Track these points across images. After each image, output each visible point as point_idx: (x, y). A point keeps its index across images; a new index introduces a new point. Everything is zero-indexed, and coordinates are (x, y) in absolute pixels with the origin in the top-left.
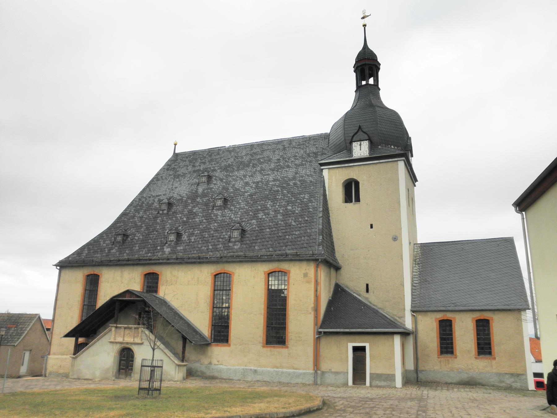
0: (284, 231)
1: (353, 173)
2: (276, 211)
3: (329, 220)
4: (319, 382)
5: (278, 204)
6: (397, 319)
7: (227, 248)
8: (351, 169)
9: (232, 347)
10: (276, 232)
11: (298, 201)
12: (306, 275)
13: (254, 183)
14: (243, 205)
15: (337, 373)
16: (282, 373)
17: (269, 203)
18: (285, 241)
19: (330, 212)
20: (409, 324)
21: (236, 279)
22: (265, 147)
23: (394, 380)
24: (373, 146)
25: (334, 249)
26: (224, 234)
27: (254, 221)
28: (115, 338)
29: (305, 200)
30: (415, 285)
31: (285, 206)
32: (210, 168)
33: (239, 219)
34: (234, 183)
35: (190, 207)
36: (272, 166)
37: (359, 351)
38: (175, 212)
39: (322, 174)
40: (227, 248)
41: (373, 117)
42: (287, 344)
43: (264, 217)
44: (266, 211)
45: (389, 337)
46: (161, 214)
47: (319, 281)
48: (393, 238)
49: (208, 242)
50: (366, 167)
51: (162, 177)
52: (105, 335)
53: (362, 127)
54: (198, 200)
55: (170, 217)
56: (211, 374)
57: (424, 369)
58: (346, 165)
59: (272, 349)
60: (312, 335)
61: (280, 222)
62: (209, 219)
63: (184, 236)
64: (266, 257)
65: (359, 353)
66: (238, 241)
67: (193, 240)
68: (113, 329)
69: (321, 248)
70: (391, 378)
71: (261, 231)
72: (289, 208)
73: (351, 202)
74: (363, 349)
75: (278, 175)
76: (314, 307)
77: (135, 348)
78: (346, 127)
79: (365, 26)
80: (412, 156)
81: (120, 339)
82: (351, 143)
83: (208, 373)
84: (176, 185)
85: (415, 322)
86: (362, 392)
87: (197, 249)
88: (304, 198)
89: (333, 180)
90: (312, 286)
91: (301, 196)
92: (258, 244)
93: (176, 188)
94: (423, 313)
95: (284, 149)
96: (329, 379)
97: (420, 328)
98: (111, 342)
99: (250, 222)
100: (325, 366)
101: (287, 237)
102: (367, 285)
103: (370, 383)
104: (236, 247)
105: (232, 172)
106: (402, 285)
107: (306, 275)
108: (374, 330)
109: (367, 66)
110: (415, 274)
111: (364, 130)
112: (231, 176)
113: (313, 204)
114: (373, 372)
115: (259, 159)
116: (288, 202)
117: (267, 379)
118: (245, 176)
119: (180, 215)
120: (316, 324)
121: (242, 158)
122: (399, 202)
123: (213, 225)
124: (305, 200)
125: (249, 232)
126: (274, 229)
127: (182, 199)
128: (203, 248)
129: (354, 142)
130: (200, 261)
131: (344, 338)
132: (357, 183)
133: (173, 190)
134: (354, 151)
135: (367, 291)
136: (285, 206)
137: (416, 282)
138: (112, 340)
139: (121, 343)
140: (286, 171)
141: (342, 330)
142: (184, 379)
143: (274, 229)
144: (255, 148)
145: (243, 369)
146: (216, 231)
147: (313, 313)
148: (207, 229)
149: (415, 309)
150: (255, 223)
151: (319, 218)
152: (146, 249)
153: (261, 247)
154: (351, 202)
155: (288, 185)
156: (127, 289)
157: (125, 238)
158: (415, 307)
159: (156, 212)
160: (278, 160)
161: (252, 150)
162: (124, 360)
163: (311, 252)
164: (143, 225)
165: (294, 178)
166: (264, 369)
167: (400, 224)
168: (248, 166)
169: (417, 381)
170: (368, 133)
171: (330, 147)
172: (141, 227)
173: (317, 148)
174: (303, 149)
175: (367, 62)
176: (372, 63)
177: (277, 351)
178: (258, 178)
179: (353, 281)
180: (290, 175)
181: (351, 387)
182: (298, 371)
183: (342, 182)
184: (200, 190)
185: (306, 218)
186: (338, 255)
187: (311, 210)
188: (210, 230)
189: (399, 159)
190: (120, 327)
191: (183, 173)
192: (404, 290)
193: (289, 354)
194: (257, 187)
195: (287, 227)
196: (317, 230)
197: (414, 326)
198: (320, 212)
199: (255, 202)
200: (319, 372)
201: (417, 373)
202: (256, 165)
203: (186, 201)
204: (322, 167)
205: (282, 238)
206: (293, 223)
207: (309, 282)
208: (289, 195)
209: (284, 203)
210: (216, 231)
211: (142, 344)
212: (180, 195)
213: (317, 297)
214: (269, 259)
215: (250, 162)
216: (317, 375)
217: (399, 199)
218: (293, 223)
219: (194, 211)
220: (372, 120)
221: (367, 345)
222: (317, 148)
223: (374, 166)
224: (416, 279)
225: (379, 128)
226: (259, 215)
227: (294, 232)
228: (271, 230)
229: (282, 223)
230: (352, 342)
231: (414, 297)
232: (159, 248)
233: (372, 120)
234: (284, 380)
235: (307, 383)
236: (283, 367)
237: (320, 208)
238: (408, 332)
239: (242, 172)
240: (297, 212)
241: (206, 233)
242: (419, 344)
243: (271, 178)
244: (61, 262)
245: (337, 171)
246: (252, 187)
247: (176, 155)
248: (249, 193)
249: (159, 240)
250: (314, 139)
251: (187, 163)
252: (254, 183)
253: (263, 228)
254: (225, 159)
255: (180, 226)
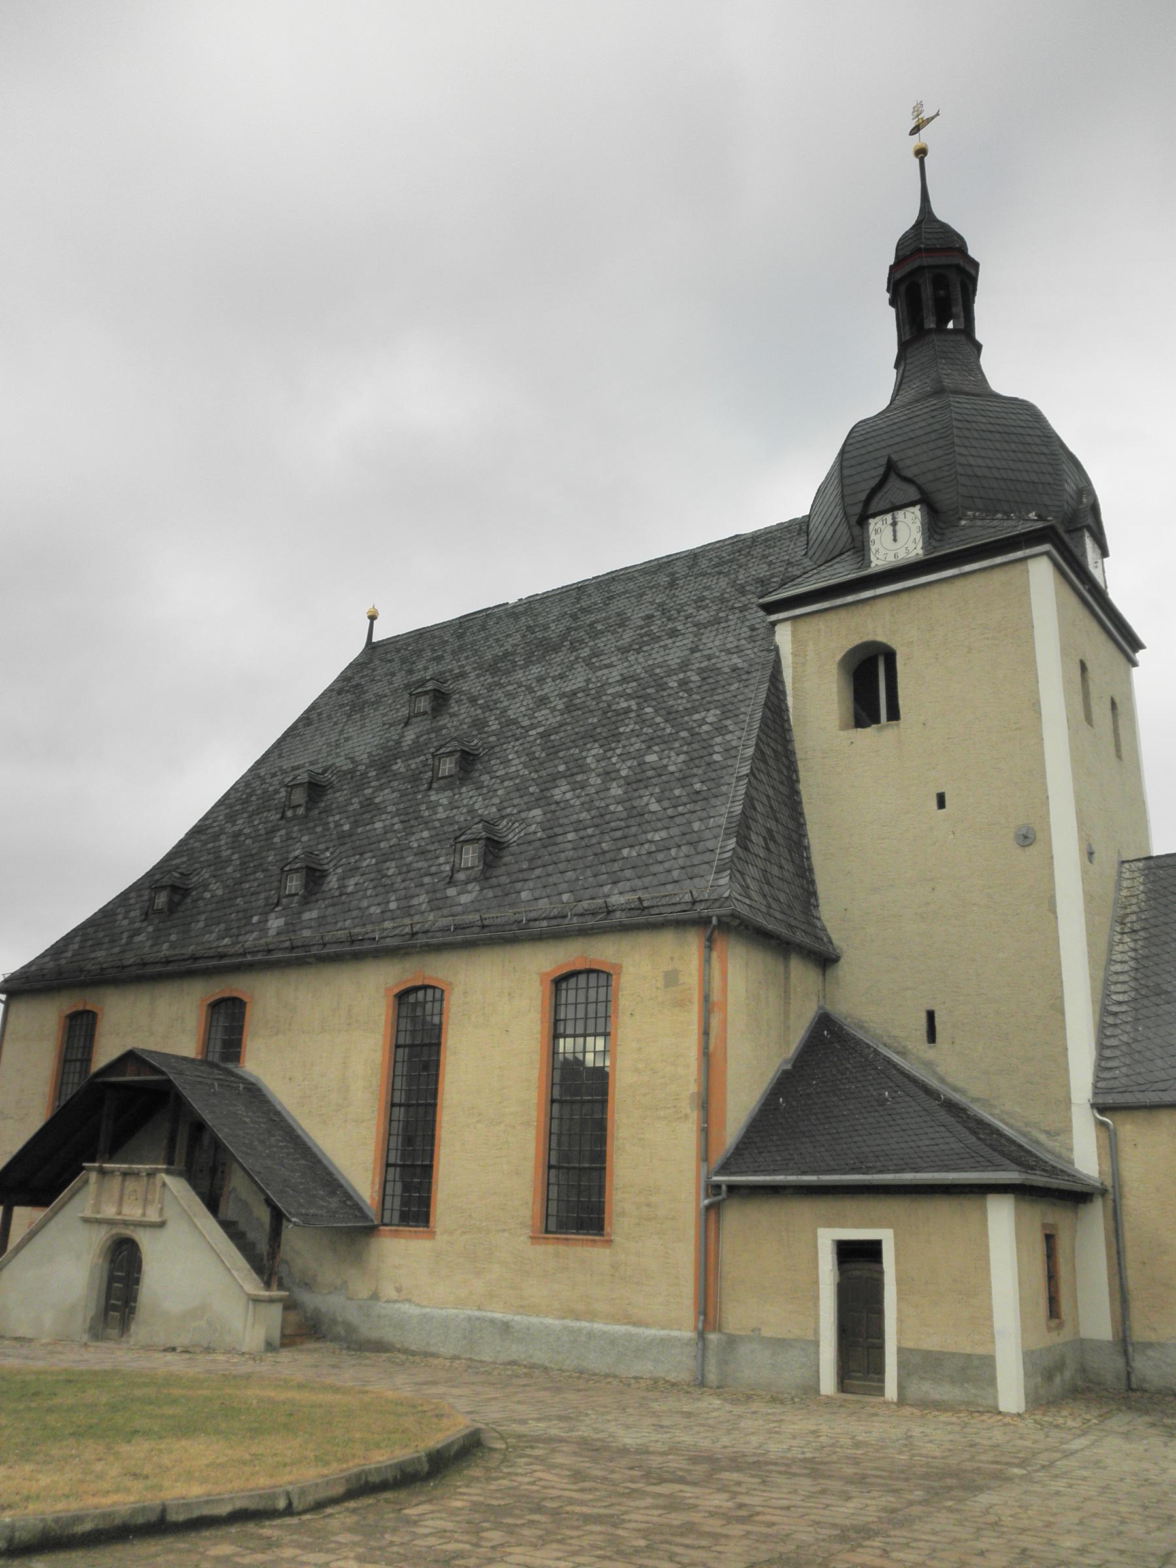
0: (619, 834)
1: (874, 622)
2: (609, 775)
3: (797, 793)
4: (712, 1377)
5: (618, 751)
6: (1043, 1138)
7: (438, 903)
8: (867, 609)
9: (441, 1239)
10: (594, 840)
11: (683, 734)
12: (671, 979)
13: (562, 695)
14: (516, 764)
15: (780, 1344)
16: (591, 1335)
17: (593, 752)
18: (616, 866)
19: (800, 765)
20: (1085, 1158)
21: (455, 1005)
22: (618, 588)
23: (992, 1381)
24: (937, 521)
25: (814, 894)
26: (442, 860)
27: (537, 812)
28: (97, 1207)
29: (705, 728)
30: (1115, 1009)
31: (640, 754)
32: (451, 671)
33: (494, 809)
34: (506, 703)
35: (368, 791)
36: (628, 637)
37: (858, 1257)
38: (327, 811)
39: (772, 642)
40: (438, 903)
41: (937, 426)
42: (607, 1229)
43: (569, 796)
44: (579, 778)
45: (968, 1204)
46: (289, 820)
47: (715, 997)
48: (1017, 835)
49: (390, 889)
50: (918, 596)
51: (320, 714)
52: (70, 1198)
53: (901, 464)
54: (395, 767)
55: (311, 825)
56: (374, 1335)
57: (1153, 1337)
58: (850, 599)
59: (562, 1248)
60: (692, 1198)
61: (612, 808)
62: (410, 818)
63: (329, 879)
64: (545, 923)
65: (860, 1269)
66: (475, 880)
67: (350, 889)
68: (93, 1176)
69: (724, 881)
70: (978, 1370)
71: (551, 839)
72: (651, 758)
73: (877, 720)
74: (870, 1252)
75: (637, 664)
76: (699, 1093)
77: (147, 1242)
78: (846, 472)
79: (921, 153)
80: (1104, 553)
81: (109, 1211)
82: (863, 520)
83: (367, 1331)
84: (351, 730)
85: (1111, 1148)
86: (878, 1428)
87: (355, 913)
88: (703, 722)
89: (810, 658)
90: (693, 1016)
91: (696, 717)
92: (531, 884)
93: (347, 739)
94: (1140, 1115)
95: (672, 584)
96: (753, 1365)
97: (1133, 1171)
98: (86, 1220)
99: (523, 815)
100: (738, 1315)
101: (625, 852)
102: (931, 1015)
103: (901, 1387)
104: (464, 899)
105: (508, 673)
106: (1058, 1008)
107: (671, 979)
108: (908, 1177)
109: (933, 283)
110: (1118, 967)
111: (907, 473)
112: (502, 686)
113: (728, 737)
114: (910, 1344)
115: (591, 625)
116: (650, 742)
117: (540, 1356)
118: (541, 680)
119: (337, 817)
120: (705, 1155)
121: (546, 627)
122: (1035, 706)
123: (417, 836)
124: (705, 728)
125: (514, 849)
126: (590, 831)
127: (352, 772)
128: (372, 910)
129: (874, 516)
130: (355, 952)
131: (802, 1211)
132: (890, 656)
133: (338, 746)
134: (873, 548)
135: (932, 1036)
136: (640, 754)
137: (1120, 998)
138: (88, 1213)
139: (110, 1222)
140: (665, 647)
141: (792, 1178)
142: (270, 1347)
143: (590, 831)
144: (590, 595)
145: (470, 1319)
146: (422, 853)
147: (694, 1115)
148: (401, 849)
149: (1109, 1100)
150: (539, 819)
151: (739, 779)
152: (222, 926)
153: (537, 894)
154: (877, 720)
155: (662, 687)
156: (129, 1048)
157: (177, 898)
158: (1109, 1091)
159: (279, 816)
160: (650, 617)
161: (578, 600)
162: (119, 1280)
163: (688, 898)
164: (236, 856)
165: (684, 666)
166: (534, 1320)
167: (1044, 784)
168: (556, 649)
169: (1130, 1388)
170: (920, 480)
171: (810, 553)
172: (229, 860)
173: (770, 564)
174: (727, 575)
175: (927, 261)
176: (943, 260)
177: (581, 1252)
178: (578, 679)
179: (877, 1000)
180: (674, 657)
181: (828, 1401)
182: (641, 1330)
183: (839, 657)
184: (410, 736)
185: (697, 786)
186: (829, 912)
187: (717, 757)
188: (405, 854)
189: (1028, 552)
190: (112, 1172)
191: (376, 695)
192: (1064, 1028)
193: (615, 1267)
194: (569, 708)
195: (632, 821)
196: (723, 821)
197: (1107, 1168)
198: (743, 760)
199: (553, 752)
200: (713, 1337)
201: (1125, 1353)
202: (582, 641)
203: (364, 774)
204: (774, 618)
205: (608, 856)
206: (654, 807)
207: (681, 1004)
208: (658, 720)
209: (637, 746)
210: (422, 853)
211: (162, 1225)
212: (353, 760)
213: (710, 1061)
214: (554, 932)
215: (563, 638)
216: (704, 1349)
217: (1037, 692)
218: (654, 807)
219: (377, 800)
220: (933, 436)
221: (886, 1236)
222: (770, 564)
223: (945, 588)
224: (1120, 988)
225: (963, 461)
226: (557, 791)
227: (650, 836)
228: (582, 833)
229: (620, 808)
230: (829, 1225)
231: (1108, 1053)
232: (255, 919)
233: (933, 436)
234: (596, 1362)
235: (672, 1377)
236: (592, 1316)
237: (745, 747)
238: (1085, 1189)
239: (536, 670)
240: (672, 768)
241: (393, 864)
242: (1129, 1236)
243: (615, 675)
244: (11, 979)
245: (820, 624)
246: (553, 710)
247: (371, 647)
248: (541, 730)
249: (262, 896)
250: (767, 540)
251: (396, 665)
252: (562, 695)
253: (558, 830)
254: (498, 640)
255: (327, 849)
